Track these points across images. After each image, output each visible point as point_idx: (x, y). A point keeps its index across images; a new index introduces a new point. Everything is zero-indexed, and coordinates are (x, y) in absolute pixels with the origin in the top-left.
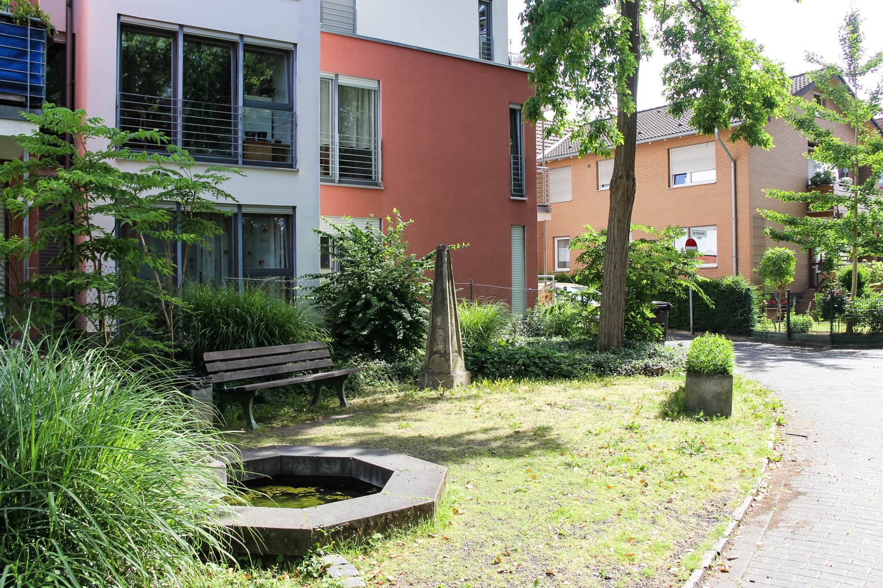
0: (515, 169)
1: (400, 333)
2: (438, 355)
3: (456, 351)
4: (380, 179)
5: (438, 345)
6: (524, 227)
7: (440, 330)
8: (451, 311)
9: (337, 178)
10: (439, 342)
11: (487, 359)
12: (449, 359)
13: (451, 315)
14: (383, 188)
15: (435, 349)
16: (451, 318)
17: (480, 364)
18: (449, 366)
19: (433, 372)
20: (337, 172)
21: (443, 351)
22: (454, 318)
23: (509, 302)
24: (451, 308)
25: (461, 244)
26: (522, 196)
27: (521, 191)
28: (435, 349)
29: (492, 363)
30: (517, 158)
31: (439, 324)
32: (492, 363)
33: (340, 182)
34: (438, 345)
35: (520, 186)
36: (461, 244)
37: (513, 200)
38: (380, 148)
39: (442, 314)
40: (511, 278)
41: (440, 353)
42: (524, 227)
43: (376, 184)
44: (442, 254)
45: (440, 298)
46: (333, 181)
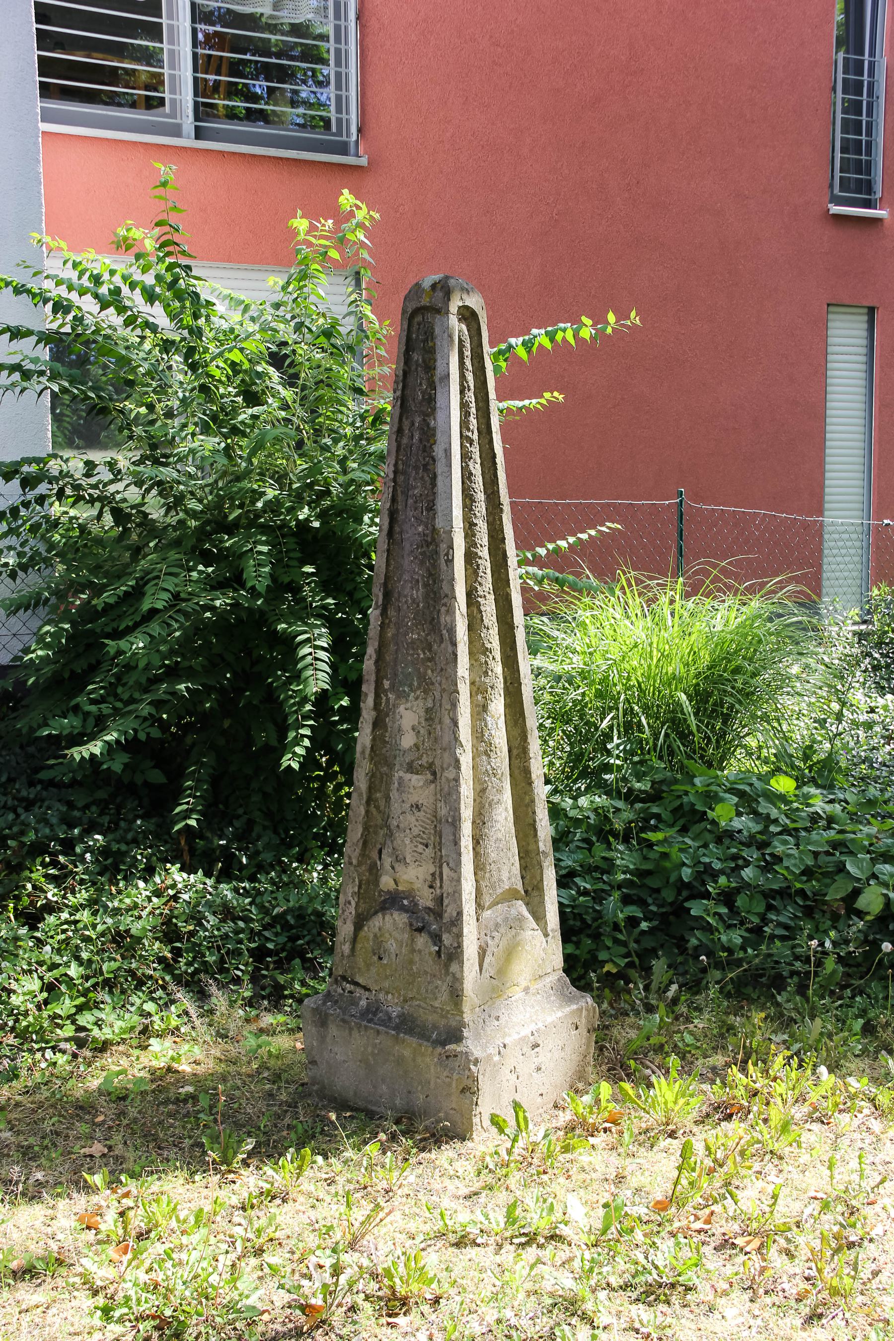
0: (847, 126)
1: (297, 741)
2: (399, 918)
3: (512, 895)
4: (354, 129)
5: (399, 859)
6: (871, 311)
7: (416, 780)
8: (479, 667)
9: (188, 122)
10: (405, 843)
11: (707, 873)
12: (455, 954)
13: (479, 690)
14: (363, 161)
15: (386, 882)
16: (481, 710)
17: (669, 895)
18: (456, 995)
19: (372, 1013)
20: (187, 97)
21: (425, 899)
22: (498, 706)
23: (815, 583)
24: (478, 649)
25: (599, 319)
26: (868, 204)
27: (868, 187)
28: (386, 882)
29: (728, 898)
30: (858, 68)
31: (407, 741)
32: (728, 898)
33: (199, 134)
34: (399, 859)
35: (866, 168)
36: (599, 319)
37: (838, 217)
38: (352, 15)
39: (426, 686)
40: (822, 486)
41: (412, 910)
42: (871, 311)
43: (343, 149)
44: (430, 335)
45: (418, 593)
46: (176, 131)
